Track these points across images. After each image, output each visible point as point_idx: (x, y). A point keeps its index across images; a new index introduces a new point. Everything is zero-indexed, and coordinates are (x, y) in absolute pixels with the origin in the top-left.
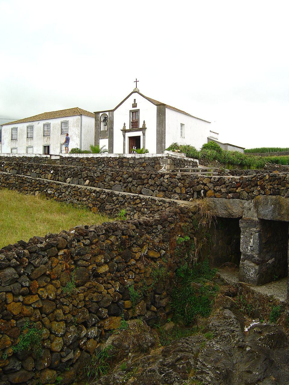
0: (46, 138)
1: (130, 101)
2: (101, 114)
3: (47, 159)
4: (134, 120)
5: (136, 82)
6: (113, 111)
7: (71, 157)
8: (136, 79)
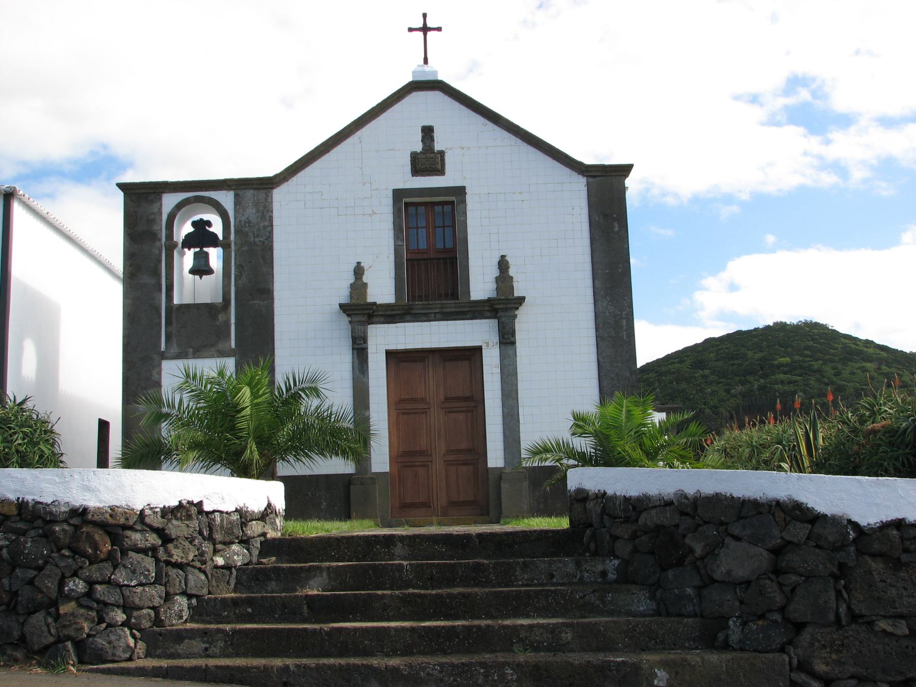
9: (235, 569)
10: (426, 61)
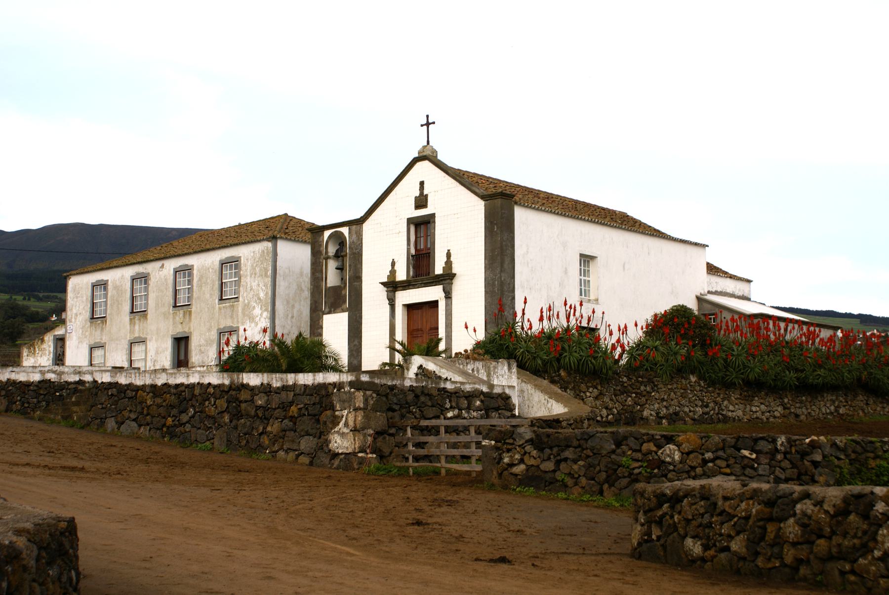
0: (182, 312)
1: (408, 189)
2: (327, 234)
3: (80, 387)
4: (421, 250)
5: (428, 124)
6: (360, 221)
7: (116, 385)
8: (428, 116)
9: (654, 451)
10: (428, 142)
